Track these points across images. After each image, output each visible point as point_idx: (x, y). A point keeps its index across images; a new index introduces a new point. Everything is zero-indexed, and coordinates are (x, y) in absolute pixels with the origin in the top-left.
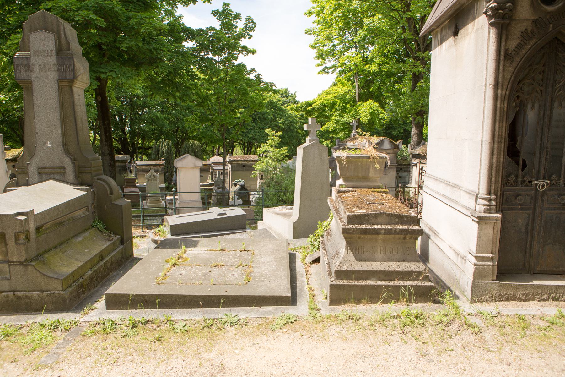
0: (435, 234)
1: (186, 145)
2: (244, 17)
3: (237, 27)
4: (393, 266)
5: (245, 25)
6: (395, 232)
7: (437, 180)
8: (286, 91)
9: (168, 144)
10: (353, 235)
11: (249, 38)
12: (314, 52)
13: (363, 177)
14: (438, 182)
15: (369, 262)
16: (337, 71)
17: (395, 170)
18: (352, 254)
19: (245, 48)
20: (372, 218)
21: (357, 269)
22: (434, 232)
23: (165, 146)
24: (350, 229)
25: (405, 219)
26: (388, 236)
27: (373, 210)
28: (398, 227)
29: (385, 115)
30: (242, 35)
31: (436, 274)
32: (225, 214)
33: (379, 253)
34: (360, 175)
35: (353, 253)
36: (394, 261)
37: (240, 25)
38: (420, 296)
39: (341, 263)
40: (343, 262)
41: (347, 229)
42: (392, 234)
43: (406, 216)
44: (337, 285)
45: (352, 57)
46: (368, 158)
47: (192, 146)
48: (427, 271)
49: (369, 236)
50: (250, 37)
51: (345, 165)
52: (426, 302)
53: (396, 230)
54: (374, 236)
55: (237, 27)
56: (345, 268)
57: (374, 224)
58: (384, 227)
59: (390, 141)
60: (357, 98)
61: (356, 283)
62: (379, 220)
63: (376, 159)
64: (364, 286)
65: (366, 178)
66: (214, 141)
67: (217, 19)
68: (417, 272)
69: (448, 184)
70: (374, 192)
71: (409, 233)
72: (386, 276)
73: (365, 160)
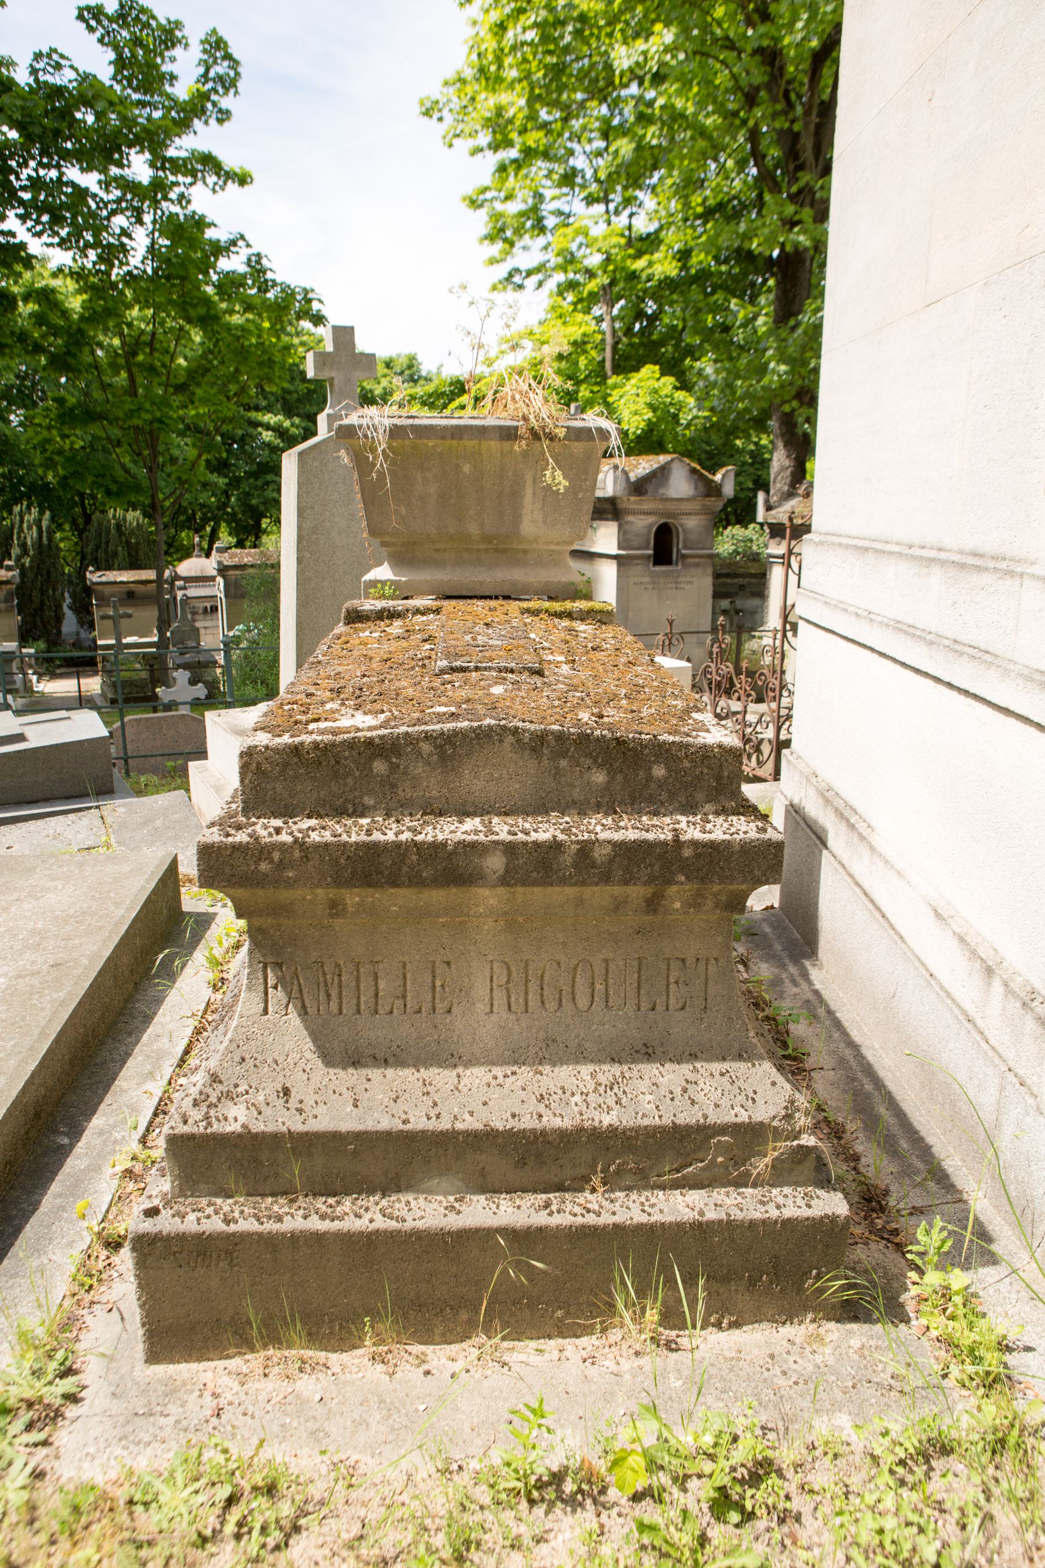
0: (852, 827)
1: (100, 524)
2: (194, 33)
3: (173, 78)
4: (574, 1095)
5: (201, 70)
6: (586, 863)
7: (863, 548)
8: (412, 363)
9: (38, 523)
10: (285, 895)
11: (220, 121)
12: (480, 221)
13: (487, 538)
14: (871, 557)
15: (408, 1073)
16: (551, 284)
17: (710, 571)
18: (294, 1017)
19: (209, 162)
20: (419, 769)
21: (323, 1121)
22: (845, 815)
23: (30, 528)
24: (258, 851)
25: (659, 771)
26: (537, 894)
27: (442, 713)
28: (606, 830)
29: (691, 409)
30: (196, 108)
31: (855, 1035)
32: (20, 738)
33: (481, 1007)
34: (473, 529)
35: (303, 1012)
36: (580, 1056)
37: (184, 69)
38: (752, 1283)
39: (215, 1079)
40: (231, 1073)
41: (237, 848)
42: (564, 881)
43: (663, 751)
44: (182, 1238)
45: (595, 229)
46: (509, 434)
47: (118, 526)
48: (802, 1120)
49: (400, 898)
50: (224, 116)
51: (381, 474)
52: (789, 1315)
53: (585, 849)
54: (438, 896)
55: (173, 78)
56: (236, 1118)
57: (436, 811)
58: (502, 829)
59: (693, 471)
60: (608, 365)
61: (316, 1224)
62: (474, 779)
63: (552, 437)
64: (372, 1240)
65: (503, 547)
66: (114, 488)
67: (101, 41)
68: (736, 1129)
69: (928, 558)
70: (535, 613)
71: (685, 867)
72: (521, 1163)
73: (494, 445)
